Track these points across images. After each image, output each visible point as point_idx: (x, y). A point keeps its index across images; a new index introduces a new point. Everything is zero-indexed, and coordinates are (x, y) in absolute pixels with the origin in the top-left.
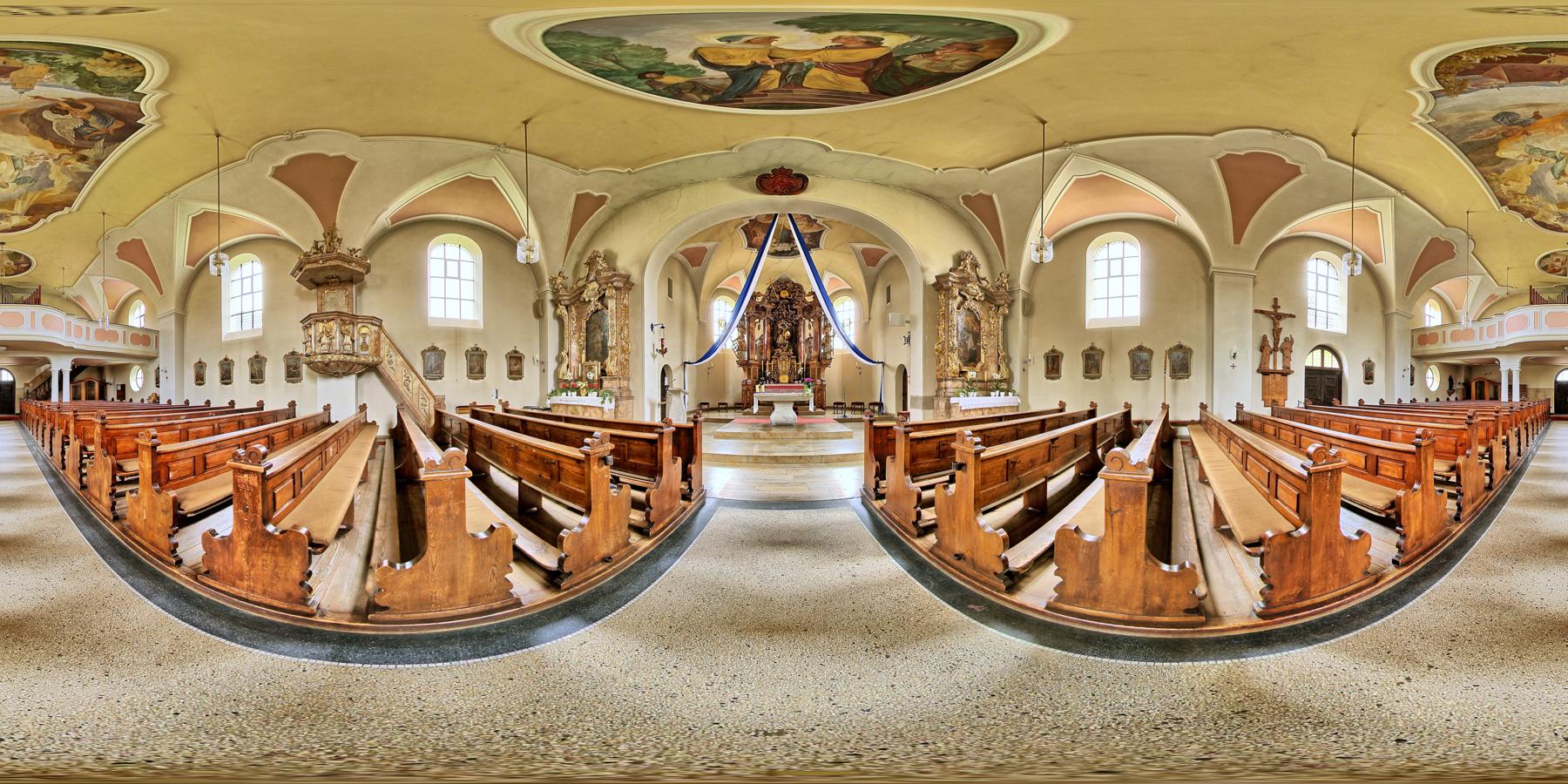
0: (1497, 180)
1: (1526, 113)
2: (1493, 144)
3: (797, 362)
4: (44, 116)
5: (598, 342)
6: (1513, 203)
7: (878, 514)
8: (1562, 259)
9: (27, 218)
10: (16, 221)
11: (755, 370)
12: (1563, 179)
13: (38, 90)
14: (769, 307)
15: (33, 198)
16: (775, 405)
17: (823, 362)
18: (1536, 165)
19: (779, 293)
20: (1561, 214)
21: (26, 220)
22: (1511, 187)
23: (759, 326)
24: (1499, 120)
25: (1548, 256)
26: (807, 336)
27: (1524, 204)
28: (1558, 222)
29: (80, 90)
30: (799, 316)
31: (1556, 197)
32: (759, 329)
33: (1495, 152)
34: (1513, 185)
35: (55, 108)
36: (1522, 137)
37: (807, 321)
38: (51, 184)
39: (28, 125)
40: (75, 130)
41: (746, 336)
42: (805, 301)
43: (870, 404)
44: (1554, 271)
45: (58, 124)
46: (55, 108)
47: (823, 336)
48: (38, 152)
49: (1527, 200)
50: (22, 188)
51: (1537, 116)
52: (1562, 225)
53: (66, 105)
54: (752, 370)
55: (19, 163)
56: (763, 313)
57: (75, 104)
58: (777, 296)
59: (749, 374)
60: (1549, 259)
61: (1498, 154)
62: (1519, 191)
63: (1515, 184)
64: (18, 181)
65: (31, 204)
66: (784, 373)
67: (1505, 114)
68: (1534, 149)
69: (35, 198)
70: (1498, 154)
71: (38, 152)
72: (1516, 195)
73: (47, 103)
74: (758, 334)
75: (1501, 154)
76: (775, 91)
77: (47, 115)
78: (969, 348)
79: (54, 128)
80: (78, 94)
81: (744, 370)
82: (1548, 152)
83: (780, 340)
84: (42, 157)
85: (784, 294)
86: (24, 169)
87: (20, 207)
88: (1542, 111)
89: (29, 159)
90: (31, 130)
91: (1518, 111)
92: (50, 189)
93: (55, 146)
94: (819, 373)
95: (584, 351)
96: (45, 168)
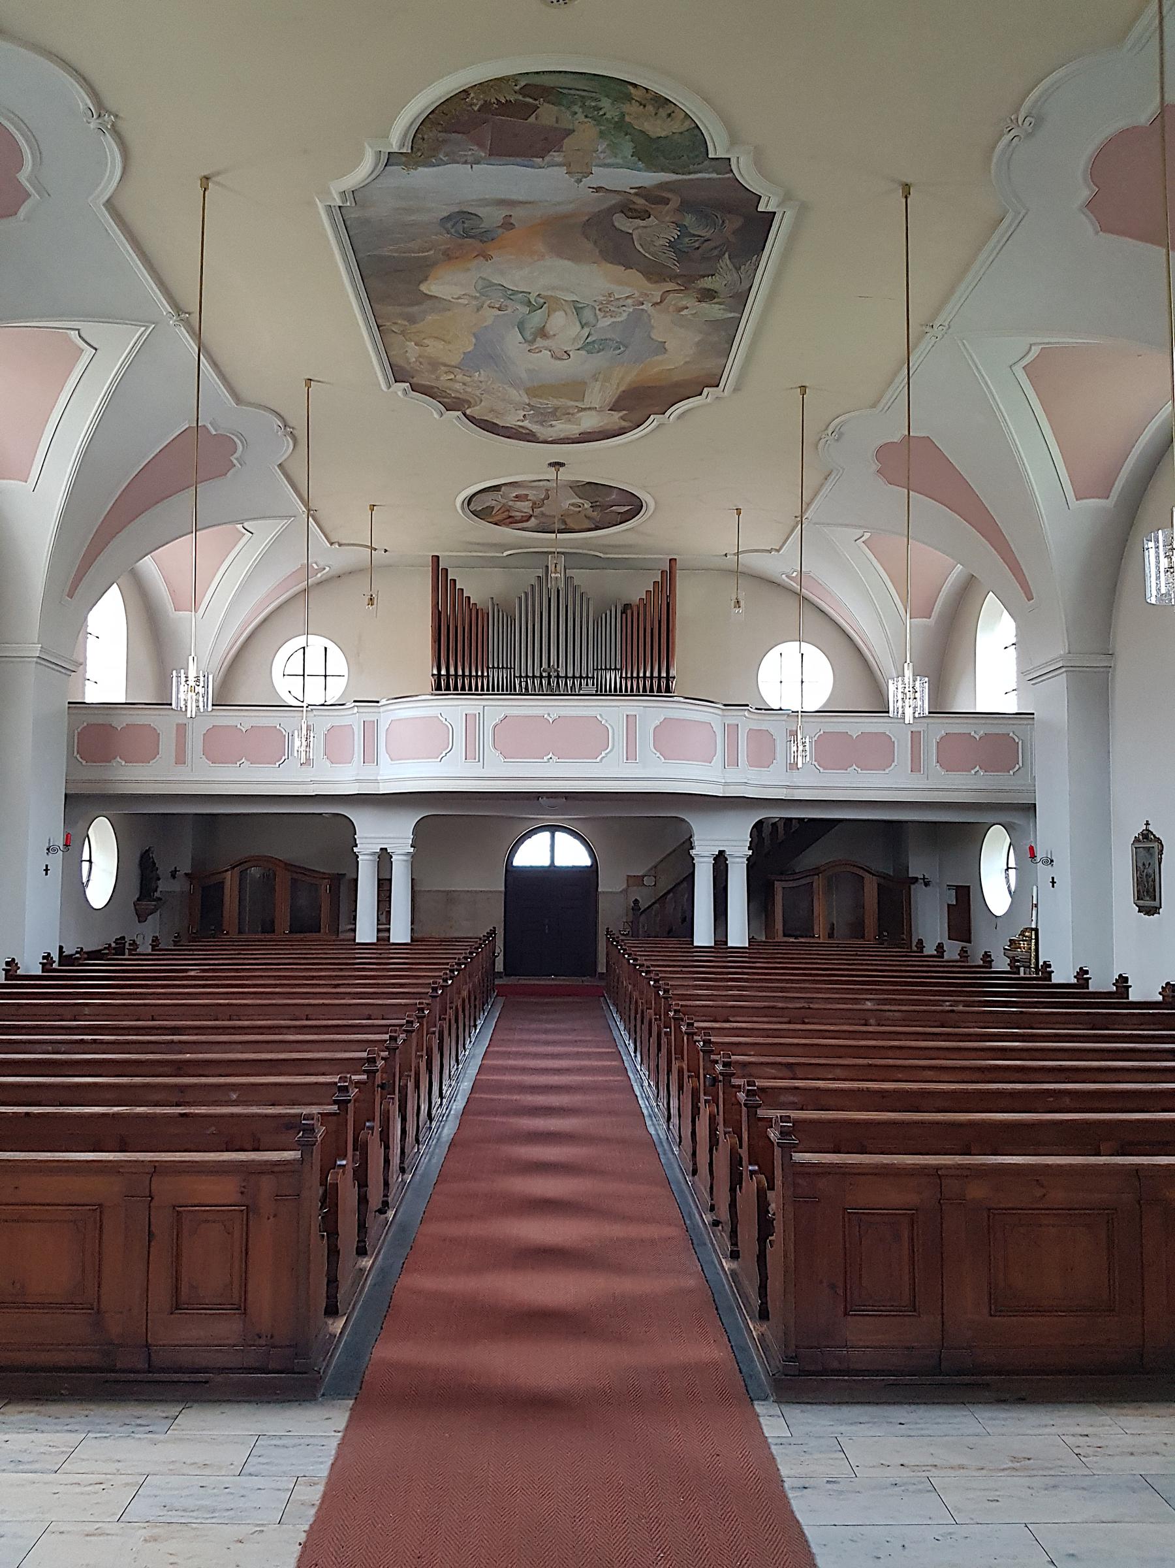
0: (403, 333)
1: (492, 217)
2: (421, 269)
4: (616, 224)
6: (423, 380)
8: (532, 494)
9: (616, 415)
10: (589, 422)
12: (540, 342)
13: (602, 176)
15: (624, 376)
18: (490, 314)
20: (532, 407)
21: (615, 419)
22: (429, 350)
24: (449, 225)
25: (496, 488)
27: (449, 384)
28: (526, 423)
29: (648, 169)
31: (524, 375)
33: (421, 282)
34: (435, 348)
35: (629, 210)
36: (475, 262)
38: (662, 348)
39: (595, 243)
40: (671, 244)
44: (509, 520)
45: (640, 238)
46: (629, 210)
48: (621, 292)
49: (459, 377)
50: (598, 361)
51: (508, 224)
52: (535, 428)
53: (641, 201)
55: (587, 315)
57: (654, 197)
60: (497, 495)
61: (423, 288)
62: (446, 360)
63: (440, 345)
64: (588, 347)
65: (622, 388)
67: (464, 215)
68: (492, 285)
69: (628, 379)
70: (423, 288)
71: (621, 292)
72: (435, 365)
73: (614, 200)
75: (431, 287)
77: (622, 222)
79: (639, 247)
80: (650, 178)
82: (515, 292)
84: (630, 301)
86: (600, 325)
87: (597, 396)
88: (518, 213)
89: (606, 306)
90: (600, 251)
91: (480, 211)
92: (659, 358)
93: (649, 280)
96: (638, 320)
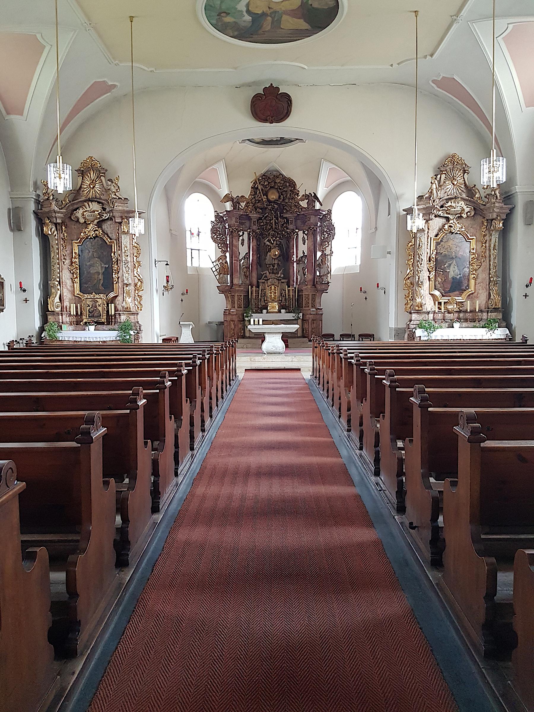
3: (289, 287)
5: (98, 273)
7: (432, 594)
11: (239, 296)
14: (254, 216)
16: (266, 335)
17: (319, 287)
19: (266, 194)
23: (243, 240)
26: (300, 254)
30: (291, 227)
32: (243, 245)
37: (301, 233)
41: (228, 255)
42: (298, 206)
43: (360, 336)
47: (319, 254)
54: (236, 298)
56: (247, 224)
58: (264, 198)
59: (233, 302)
66: (273, 301)
74: (243, 250)
76: (268, 31)
78: (450, 277)
81: (226, 297)
83: (268, 260)
85: (273, 196)
94: (314, 300)
95: (77, 280)
